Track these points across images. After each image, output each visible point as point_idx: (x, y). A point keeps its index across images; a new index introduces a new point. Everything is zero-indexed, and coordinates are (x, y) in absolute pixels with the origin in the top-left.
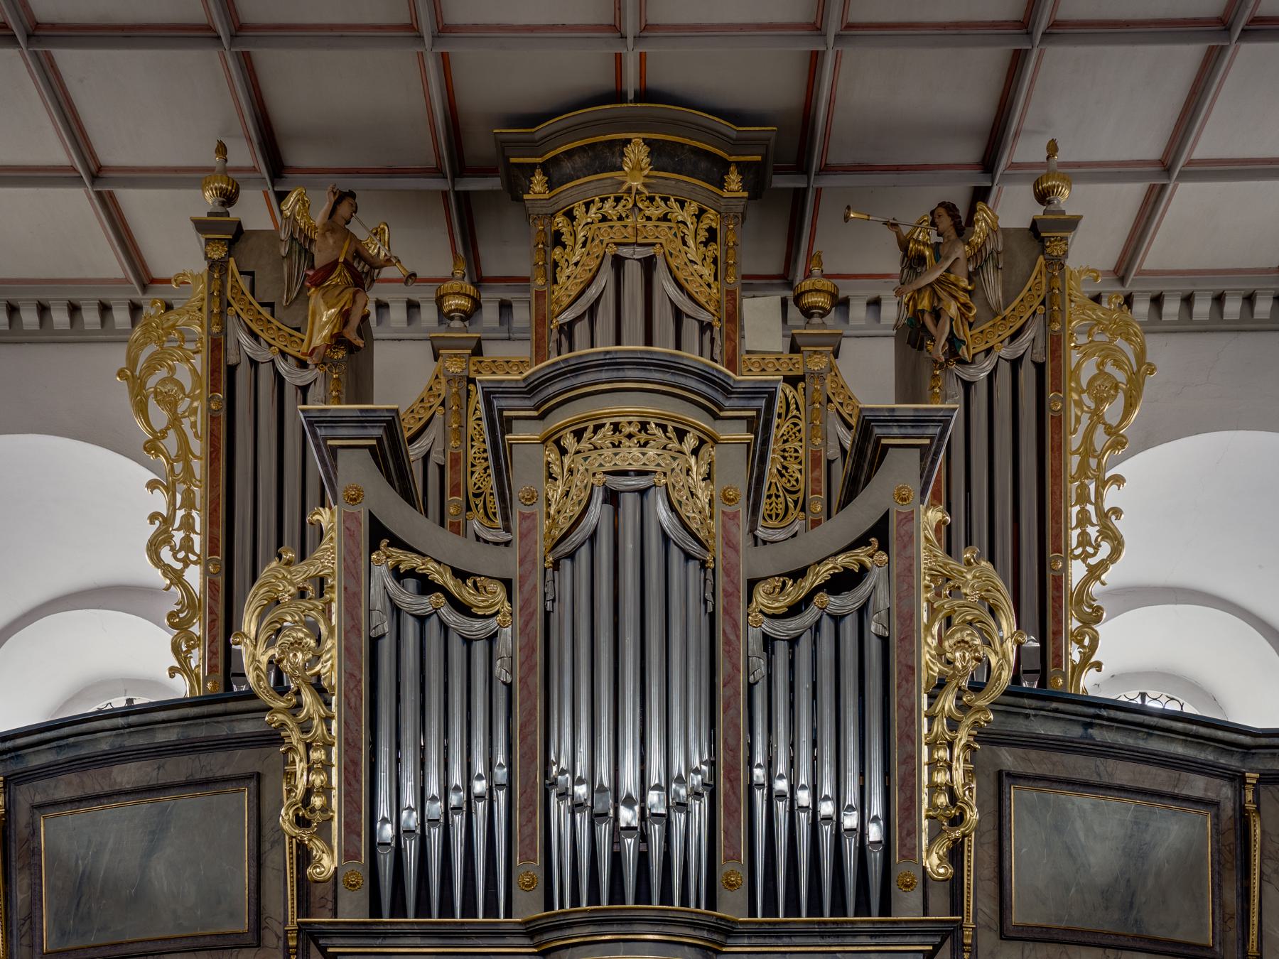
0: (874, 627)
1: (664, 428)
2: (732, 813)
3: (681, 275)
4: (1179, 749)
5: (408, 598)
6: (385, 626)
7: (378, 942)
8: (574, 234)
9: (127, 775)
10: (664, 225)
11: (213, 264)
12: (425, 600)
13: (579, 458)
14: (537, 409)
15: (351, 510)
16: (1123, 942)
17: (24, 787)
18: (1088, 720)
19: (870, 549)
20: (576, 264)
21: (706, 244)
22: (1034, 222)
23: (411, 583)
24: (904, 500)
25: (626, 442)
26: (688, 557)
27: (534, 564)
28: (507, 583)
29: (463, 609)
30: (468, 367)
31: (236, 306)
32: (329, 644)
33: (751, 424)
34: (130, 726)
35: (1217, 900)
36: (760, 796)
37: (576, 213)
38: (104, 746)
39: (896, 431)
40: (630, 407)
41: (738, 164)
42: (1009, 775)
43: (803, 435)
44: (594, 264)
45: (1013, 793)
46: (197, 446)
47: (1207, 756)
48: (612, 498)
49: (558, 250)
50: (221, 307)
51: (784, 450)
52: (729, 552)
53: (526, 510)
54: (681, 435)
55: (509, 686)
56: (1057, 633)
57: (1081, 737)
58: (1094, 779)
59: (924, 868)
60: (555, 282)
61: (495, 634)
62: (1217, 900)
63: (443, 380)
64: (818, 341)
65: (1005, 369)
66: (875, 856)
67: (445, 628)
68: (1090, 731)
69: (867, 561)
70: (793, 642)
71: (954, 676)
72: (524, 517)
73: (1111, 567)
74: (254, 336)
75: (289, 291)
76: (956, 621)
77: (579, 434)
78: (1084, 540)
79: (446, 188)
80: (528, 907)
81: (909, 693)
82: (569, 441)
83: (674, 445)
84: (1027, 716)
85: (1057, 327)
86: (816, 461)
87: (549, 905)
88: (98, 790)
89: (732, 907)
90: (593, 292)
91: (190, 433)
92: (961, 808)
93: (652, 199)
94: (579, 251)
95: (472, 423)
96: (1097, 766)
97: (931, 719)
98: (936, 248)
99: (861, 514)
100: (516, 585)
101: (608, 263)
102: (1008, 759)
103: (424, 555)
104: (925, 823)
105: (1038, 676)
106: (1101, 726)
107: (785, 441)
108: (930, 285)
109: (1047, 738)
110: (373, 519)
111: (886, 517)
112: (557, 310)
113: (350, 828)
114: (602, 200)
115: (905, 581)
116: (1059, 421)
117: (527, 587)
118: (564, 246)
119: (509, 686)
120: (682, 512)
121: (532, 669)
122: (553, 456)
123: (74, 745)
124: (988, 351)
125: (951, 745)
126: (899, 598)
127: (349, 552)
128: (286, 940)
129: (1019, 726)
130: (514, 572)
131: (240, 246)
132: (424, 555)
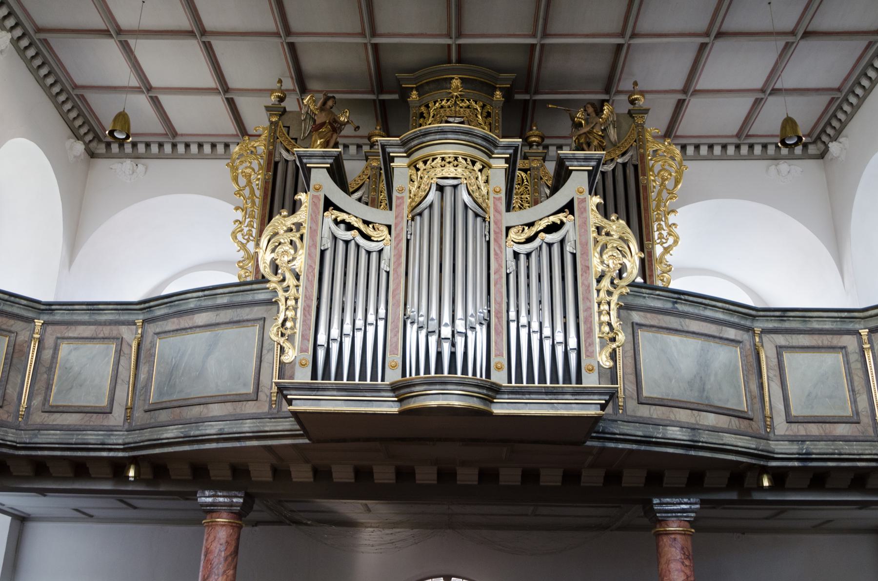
0: (569, 248)
1: (466, 160)
2: (498, 313)
4: (720, 315)
5: (342, 234)
6: (328, 244)
7: (314, 393)
9: (201, 319)
10: (468, 110)
11: (272, 123)
12: (349, 233)
13: (425, 172)
14: (405, 152)
15: (316, 194)
17: (151, 325)
21: (486, 117)
22: (629, 111)
23: (342, 226)
25: (447, 165)
26: (477, 215)
27: (402, 218)
28: (389, 227)
29: (368, 238)
32: (300, 252)
33: (507, 160)
36: (513, 326)
38: (192, 306)
39: (576, 163)
40: (450, 150)
41: (500, 88)
42: (637, 324)
45: (640, 333)
46: (258, 193)
47: (735, 319)
48: (441, 189)
50: (273, 139)
52: (497, 214)
53: (399, 195)
54: (474, 163)
55: (388, 273)
56: (651, 276)
58: (679, 328)
61: (382, 249)
64: (536, 155)
65: (620, 168)
66: (573, 357)
67: (358, 246)
69: (565, 220)
70: (528, 255)
71: (609, 271)
72: (398, 198)
74: (288, 151)
76: (609, 246)
77: (425, 162)
78: (661, 237)
79: (365, 41)
81: (587, 279)
82: (420, 165)
83: (470, 166)
84: (644, 297)
88: (187, 326)
89: (499, 377)
91: (255, 188)
95: (381, 185)
97: (598, 291)
102: (636, 317)
103: (349, 214)
104: (598, 340)
108: (585, 133)
110: (326, 199)
111: (572, 201)
113: (304, 337)
114: (442, 100)
116: (646, 188)
117: (398, 228)
118: (424, 118)
119: (388, 273)
120: (474, 195)
121: (400, 264)
122: (414, 171)
123: (178, 305)
126: (580, 236)
127: (314, 212)
128: (271, 397)
129: (640, 302)
132: (349, 214)
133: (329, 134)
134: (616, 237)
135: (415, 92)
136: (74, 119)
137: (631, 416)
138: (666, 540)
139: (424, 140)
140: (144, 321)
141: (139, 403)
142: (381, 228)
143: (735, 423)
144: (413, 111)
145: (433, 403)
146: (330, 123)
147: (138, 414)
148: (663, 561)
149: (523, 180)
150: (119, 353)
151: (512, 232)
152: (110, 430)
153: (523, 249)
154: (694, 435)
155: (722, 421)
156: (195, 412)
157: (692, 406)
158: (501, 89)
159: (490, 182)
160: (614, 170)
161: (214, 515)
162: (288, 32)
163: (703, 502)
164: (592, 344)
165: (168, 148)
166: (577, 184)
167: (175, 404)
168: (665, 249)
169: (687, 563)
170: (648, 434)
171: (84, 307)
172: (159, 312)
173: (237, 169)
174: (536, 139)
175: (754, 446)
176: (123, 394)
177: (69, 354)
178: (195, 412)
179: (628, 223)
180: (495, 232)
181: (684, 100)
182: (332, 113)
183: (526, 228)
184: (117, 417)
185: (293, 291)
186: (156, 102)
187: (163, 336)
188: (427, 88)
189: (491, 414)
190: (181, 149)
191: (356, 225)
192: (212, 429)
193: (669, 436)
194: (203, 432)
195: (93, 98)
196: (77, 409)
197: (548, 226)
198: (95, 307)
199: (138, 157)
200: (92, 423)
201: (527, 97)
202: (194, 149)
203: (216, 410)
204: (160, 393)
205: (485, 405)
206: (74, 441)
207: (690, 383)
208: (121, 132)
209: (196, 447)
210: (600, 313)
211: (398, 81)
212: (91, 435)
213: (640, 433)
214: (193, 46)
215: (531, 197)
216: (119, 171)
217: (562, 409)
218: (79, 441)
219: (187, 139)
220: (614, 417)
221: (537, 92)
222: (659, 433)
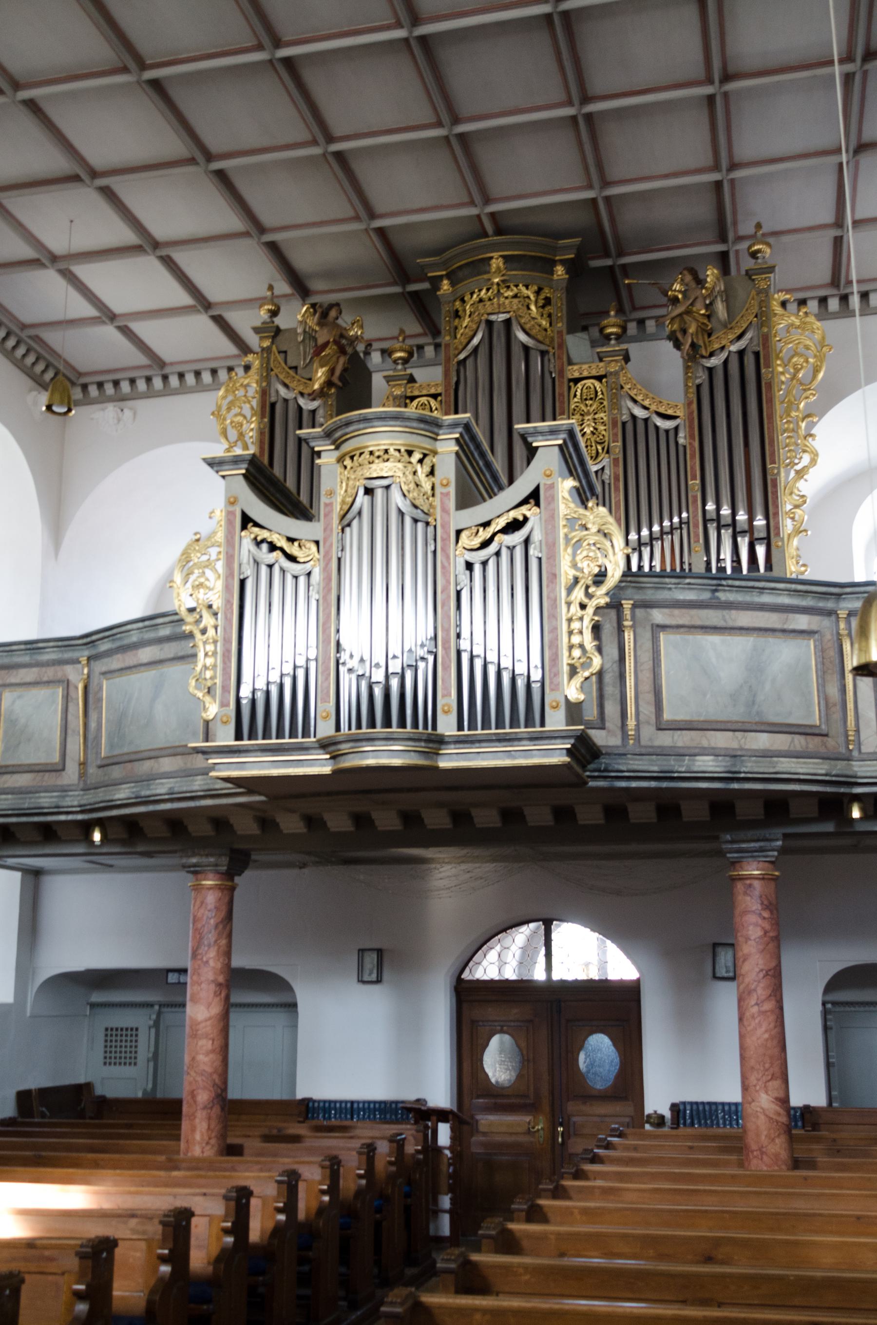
0: (533, 552)
1: (399, 451)
2: (446, 668)
3: (527, 327)
4: (785, 600)
5: (266, 556)
6: (248, 571)
8: (465, 310)
9: (146, 654)
10: (516, 301)
15: (231, 509)
16: (748, 727)
17: (97, 663)
18: (714, 588)
19: (528, 506)
20: (466, 327)
21: (543, 307)
24: (548, 476)
25: (377, 461)
27: (332, 530)
28: (317, 543)
29: (292, 559)
30: (406, 390)
31: (276, 371)
34: (145, 627)
35: (821, 695)
37: (466, 299)
38: (134, 639)
42: (658, 626)
43: (606, 409)
44: (475, 327)
48: (369, 491)
49: (457, 320)
51: (595, 419)
53: (328, 501)
56: (776, 514)
57: (711, 599)
58: (721, 624)
59: (566, 696)
60: (456, 338)
62: (821, 695)
63: (391, 398)
68: (717, 594)
69: (528, 514)
70: (484, 563)
71: (583, 577)
72: (326, 505)
73: (811, 470)
74: (286, 386)
75: (305, 359)
77: (352, 458)
80: (325, 729)
84: (670, 589)
85: (765, 330)
86: (614, 423)
87: (338, 728)
88: (131, 663)
90: (476, 341)
92: (589, 657)
93: (508, 287)
94: (467, 320)
96: (723, 616)
97: (569, 604)
98: (684, 293)
99: (522, 487)
100: (321, 544)
101: (483, 326)
105: (766, 541)
106: (725, 591)
107: (596, 414)
109: (684, 601)
112: (457, 352)
113: (225, 689)
114: (480, 291)
115: (551, 521)
117: (328, 544)
118: (460, 317)
123: (120, 639)
124: (723, 348)
125: (581, 619)
126: (547, 534)
130: (320, 537)
131: (279, 338)
133: (334, 359)
134: (594, 529)
135: (445, 282)
136: (34, 364)
137: (646, 747)
138: (739, 886)
139: (347, 430)
140: (89, 659)
141: (91, 757)
142: (308, 545)
143: (799, 743)
144: (445, 308)
145: (371, 762)
146: (336, 342)
147: (92, 770)
148: (737, 912)
149: (596, 392)
150: (67, 698)
151: (464, 535)
152: (64, 790)
153: (476, 558)
154: (734, 765)
155: (781, 742)
156: (146, 767)
157: (734, 727)
158: (563, 262)
159: (436, 473)
160: (726, 362)
161: (203, 876)
162: (262, 229)
163: (786, 836)
164: (557, 674)
165: (158, 383)
166: (546, 467)
167: (126, 758)
168: (797, 472)
169: (766, 914)
170: (666, 768)
171: (23, 647)
172: (104, 646)
173: (225, 419)
174: (614, 330)
175: (823, 772)
176: (75, 746)
177: (14, 702)
178: (146, 767)
179: (610, 511)
180: (443, 540)
181: (842, 237)
182: (338, 326)
183: (481, 529)
184: (71, 775)
185: (211, 632)
186: (125, 331)
187: (108, 676)
188: (460, 274)
189: (437, 768)
190: (174, 381)
191: (279, 545)
192: (161, 788)
193: (696, 769)
194: (154, 792)
195: (53, 338)
196: (26, 768)
197: (508, 524)
198: (35, 646)
199: (123, 399)
200: (44, 784)
201: (609, 262)
202: (190, 379)
203: (167, 764)
204: (111, 746)
205: (426, 759)
206: (26, 806)
207: (734, 697)
208: (61, 404)
209: (151, 808)
210: (570, 633)
211: (422, 267)
212: (44, 797)
213: (656, 768)
214: (150, 263)
215: (608, 416)
216: (99, 419)
217: (520, 757)
218: (32, 806)
219: (180, 368)
220: (622, 751)
221: (621, 254)
222: (681, 767)
